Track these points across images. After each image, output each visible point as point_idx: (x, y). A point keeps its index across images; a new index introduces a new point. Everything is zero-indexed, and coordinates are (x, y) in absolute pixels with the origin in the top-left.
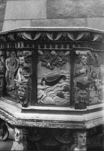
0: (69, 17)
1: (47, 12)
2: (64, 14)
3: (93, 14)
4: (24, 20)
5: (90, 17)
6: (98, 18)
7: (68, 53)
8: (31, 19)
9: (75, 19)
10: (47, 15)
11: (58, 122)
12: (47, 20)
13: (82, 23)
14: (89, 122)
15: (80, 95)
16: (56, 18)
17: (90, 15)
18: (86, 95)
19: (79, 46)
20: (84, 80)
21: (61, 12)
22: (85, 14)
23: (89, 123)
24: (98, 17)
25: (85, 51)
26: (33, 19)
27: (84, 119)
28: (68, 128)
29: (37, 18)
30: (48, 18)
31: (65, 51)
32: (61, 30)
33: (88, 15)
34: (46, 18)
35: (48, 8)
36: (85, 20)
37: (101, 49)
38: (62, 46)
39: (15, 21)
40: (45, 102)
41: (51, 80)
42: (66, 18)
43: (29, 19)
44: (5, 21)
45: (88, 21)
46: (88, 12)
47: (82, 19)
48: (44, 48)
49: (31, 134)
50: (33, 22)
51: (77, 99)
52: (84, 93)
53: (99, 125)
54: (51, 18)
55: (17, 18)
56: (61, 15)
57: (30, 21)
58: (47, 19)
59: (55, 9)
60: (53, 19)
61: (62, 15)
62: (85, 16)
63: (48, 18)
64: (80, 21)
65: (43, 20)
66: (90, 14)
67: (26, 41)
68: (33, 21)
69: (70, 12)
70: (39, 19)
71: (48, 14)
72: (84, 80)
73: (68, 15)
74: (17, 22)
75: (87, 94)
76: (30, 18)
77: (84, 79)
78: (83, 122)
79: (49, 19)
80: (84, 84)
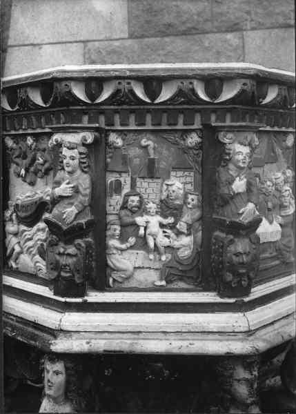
0: (194, 32)
1: (129, 21)
2: (176, 22)
3: (260, 20)
4: (64, 45)
5: (253, 29)
6: (276, 30)
7: (193, 139)
8: (83, 42)
9: (209, 35)
10: (129, 27)
11: (17, 321)
12: (129, 42)
13: (231, 45)
14: (75, 336)
15: (58, 257)
16: (157, 36)
17: (253, 22)
18: (75, 259)
19: (228, 117)
20: (65, 216)
21: (168, 18)
22: (237, 21)
23: (74, 338)
24: (277, 28)
25: (76, 135)
26: (88, 41)
27: (58, 323)
28: (19, 338)
29: (102, 37)
30: (131, 36)
31: (186, 133)
32: (113, 74)
33: (248, 23)
34: (127, 36)
35: (130, 9)
36: (239, 38)
37: (8, 129)
38: (132, 119)
39: (40, 48)
40: (133, 284)
41: (26, 211)
42: (184, 33)
43: (78, 40)
44: (9, 50)
45: (247, 39)
46: (245, 16)
47: (229, 36)
48: (224, 122)
49: (99, 373)
50: (89, 50)
51: (52, 266)
52: (66, 253)
53: (105, 351)
54: (143, 37)
55: (43, 40)
56: (169, 25)
57: (82, 45)
58: (129, 38)
59: (151, 8)
60: (147, 39)
61: (172, 26)
62: (236, 27)
63: (131, 36)
64: (226, 41)
65: (117, 43)
66: (252, 20)
67: (146, 107)
68: (90, 45)
69: (195, 17)
70: (107, 40)
71: (131, 25)
72: (65, 216)
73: (189, 25)
74: (43, 50)
75: (79, 256)
76: (82, 39)
77: (64, 213)
78: (54, 333)
79: (137, 37)
80: (65, 228)
